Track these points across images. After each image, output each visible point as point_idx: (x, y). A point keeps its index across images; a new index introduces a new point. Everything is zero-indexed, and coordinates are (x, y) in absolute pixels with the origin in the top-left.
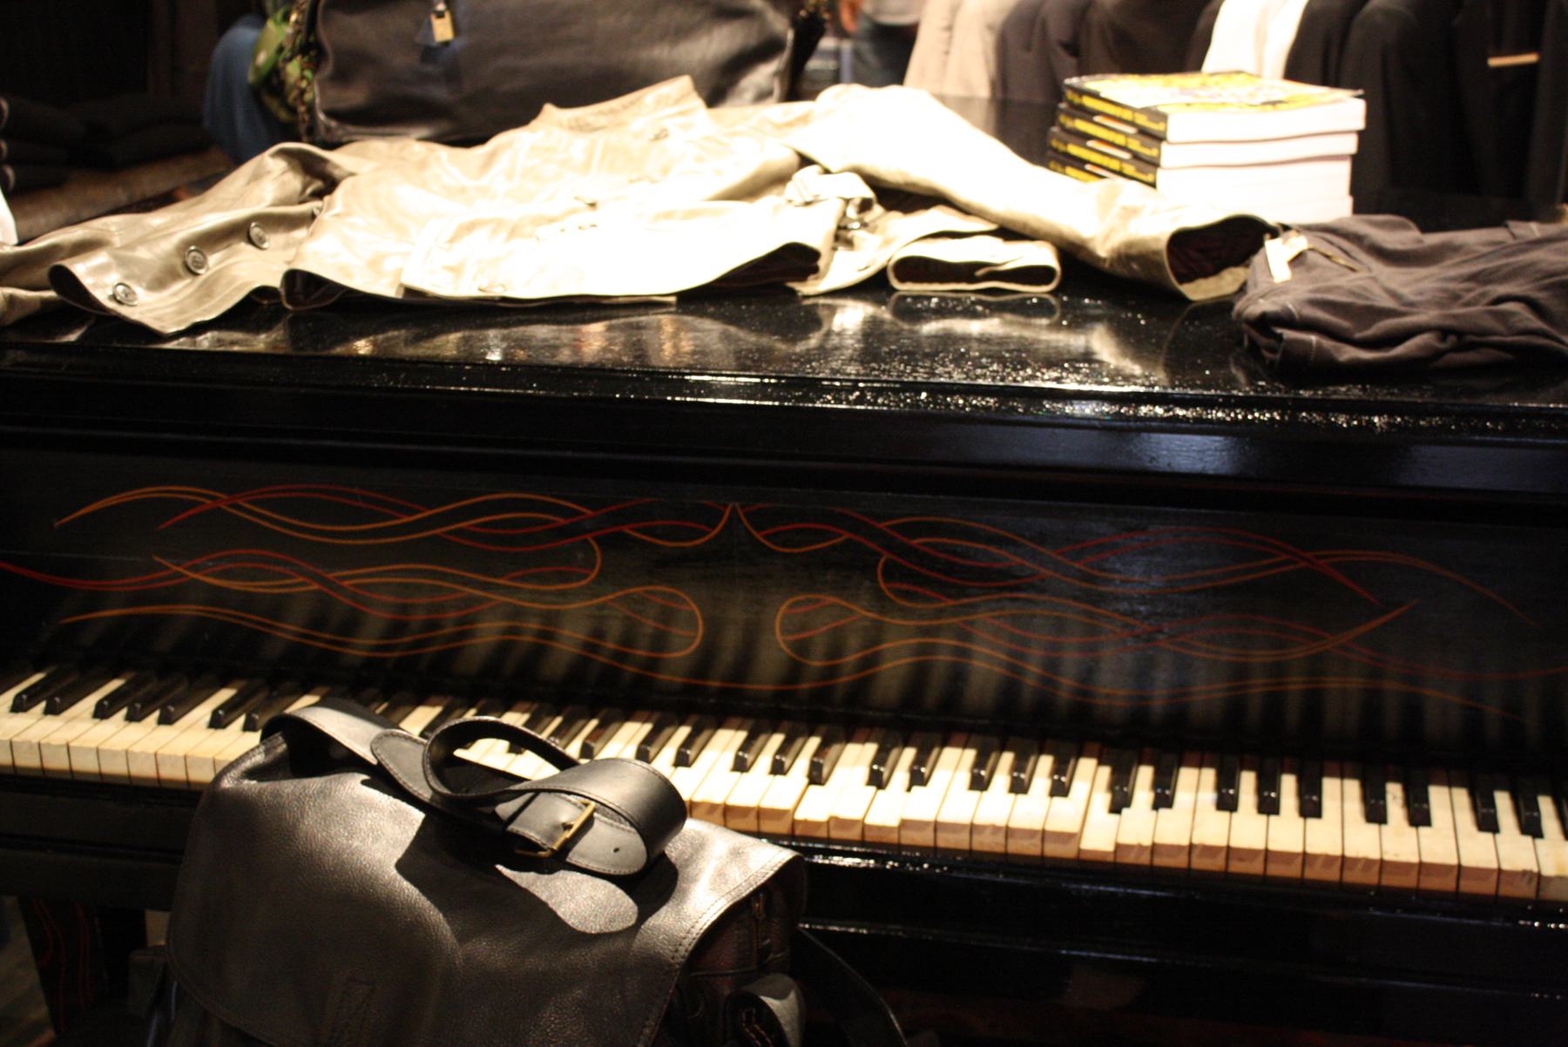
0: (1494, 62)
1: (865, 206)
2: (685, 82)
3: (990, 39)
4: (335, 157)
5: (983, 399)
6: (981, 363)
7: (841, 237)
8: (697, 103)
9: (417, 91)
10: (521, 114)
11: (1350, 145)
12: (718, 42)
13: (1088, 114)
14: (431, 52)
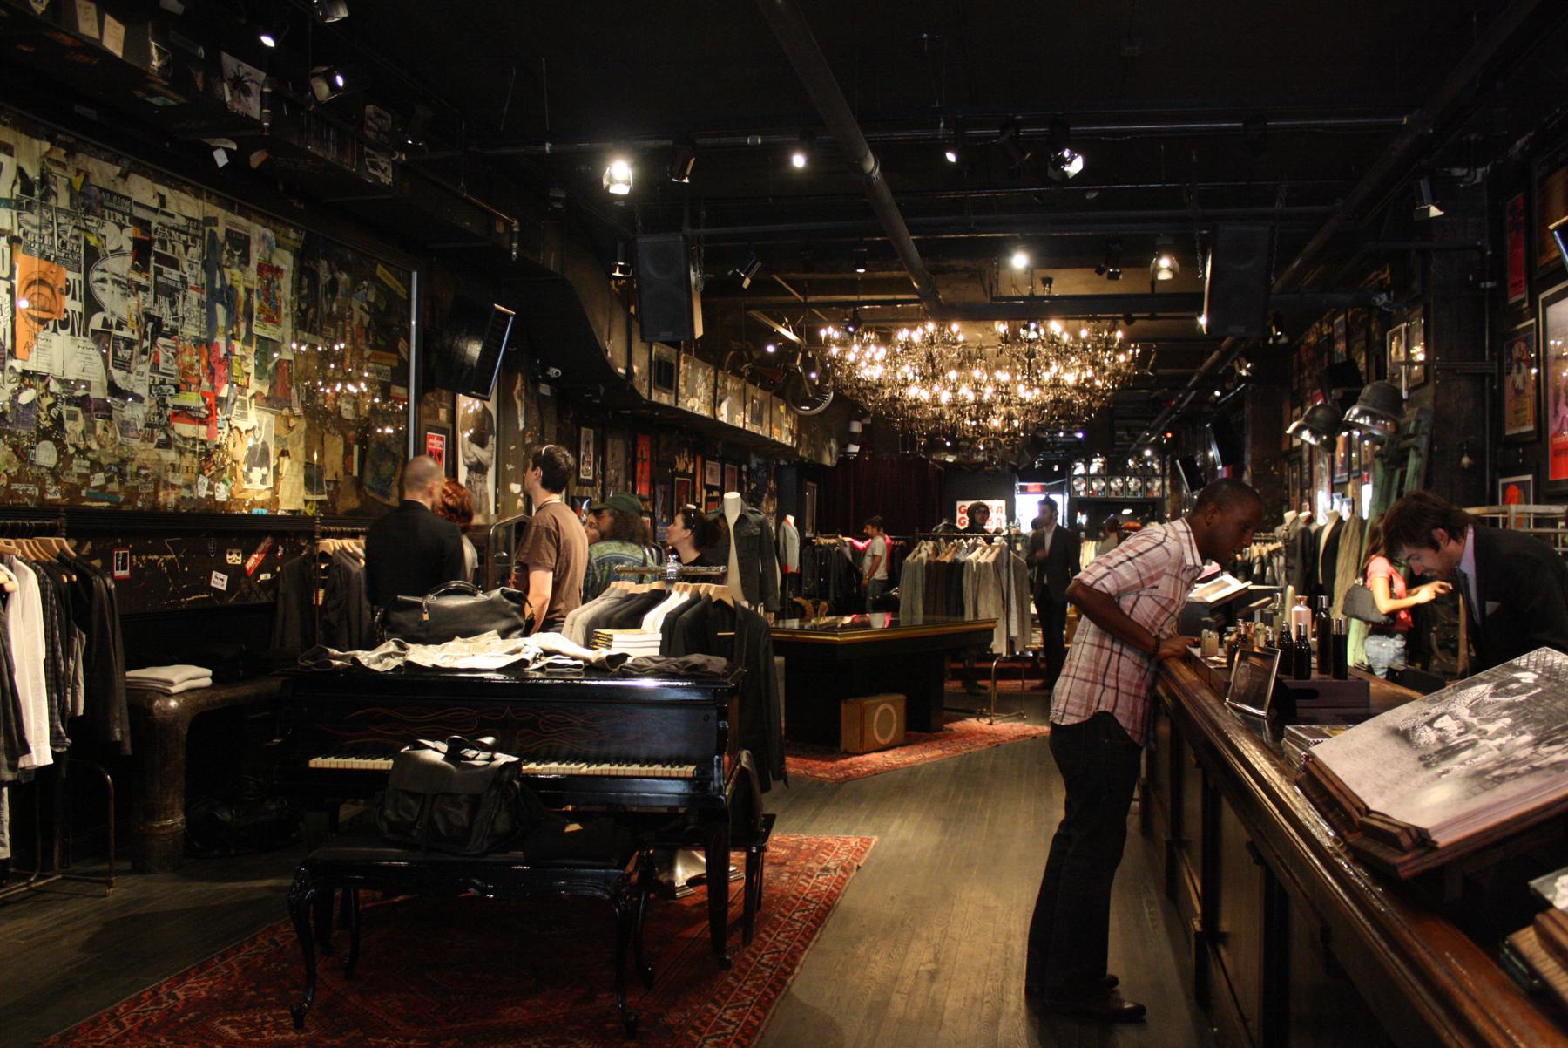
0: (318, 762)
1: (541, 655)
2: (495, 632)
3: (584, 628)
4: (409, 645)
5: (1056, 384)
6: (1360, 431)
7: (535, 660)
8: (499, 637)
9: (416, 634)
10: (450, 638)
11: (659, 644)
12: (504, 624)
13: (598, 638)
14: (422, 623)
